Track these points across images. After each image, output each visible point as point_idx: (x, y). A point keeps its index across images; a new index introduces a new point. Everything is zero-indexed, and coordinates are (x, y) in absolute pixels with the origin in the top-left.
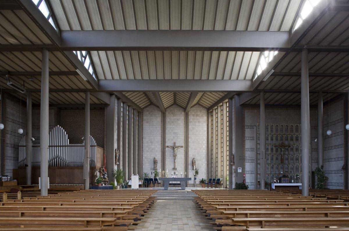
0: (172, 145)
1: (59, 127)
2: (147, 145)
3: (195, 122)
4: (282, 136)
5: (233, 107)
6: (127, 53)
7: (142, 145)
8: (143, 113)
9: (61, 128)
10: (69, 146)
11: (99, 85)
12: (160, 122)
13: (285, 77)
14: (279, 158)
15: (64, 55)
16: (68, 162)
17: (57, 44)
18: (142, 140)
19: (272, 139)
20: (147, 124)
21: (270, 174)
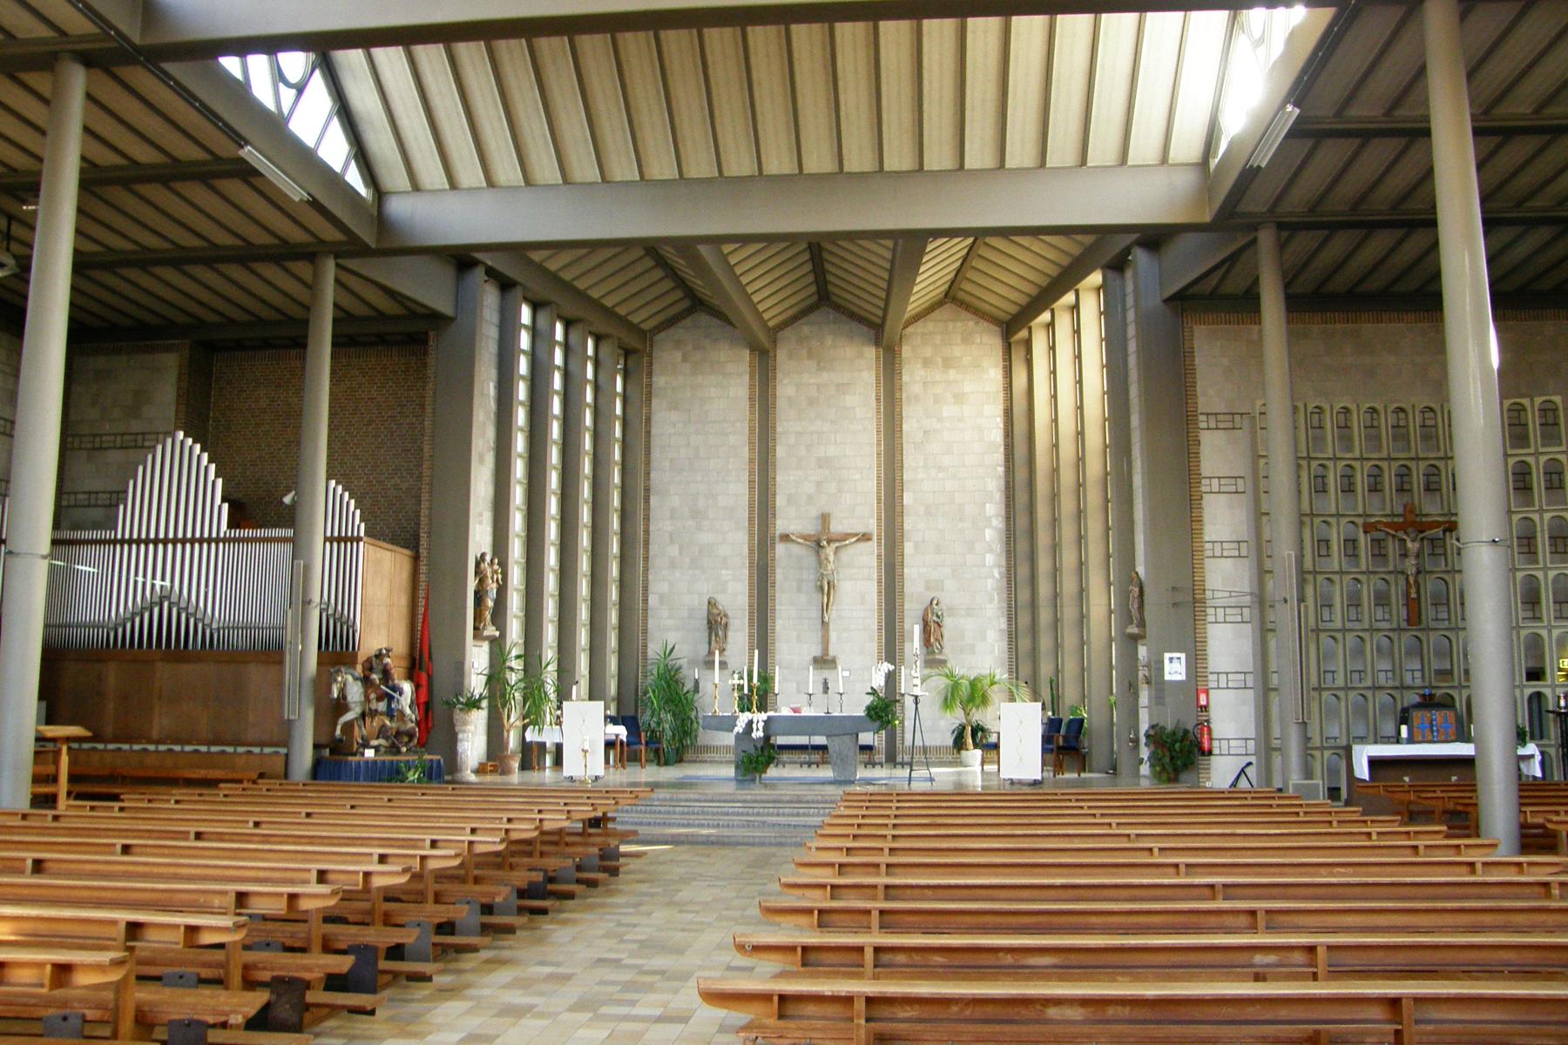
0: (810, 528)
1: (182, 442)
2: (669, 529)
3: (937, 400)
4: (1405, 471)
5: (1131, 315)
6: (513, 51)
7: (647, 532)
8: (650, 355)
9: (191, 448)
10: (225, 540)
11: (381, 221)
12: (745, 404)
13: (1376, 140)
14: (1396, 593)
15: (165, 78)
16: (215, 626)
17: (118, 32)
18: (647, 500)
19: (1349, 489)
20: (674, 416)
21: (1347, 689)
